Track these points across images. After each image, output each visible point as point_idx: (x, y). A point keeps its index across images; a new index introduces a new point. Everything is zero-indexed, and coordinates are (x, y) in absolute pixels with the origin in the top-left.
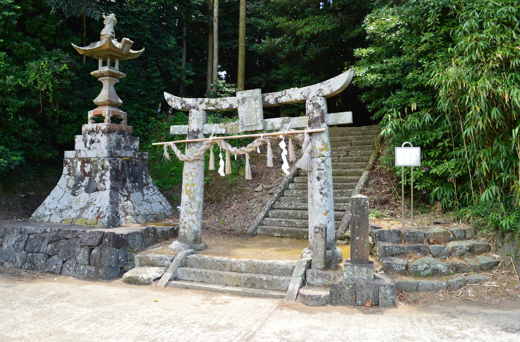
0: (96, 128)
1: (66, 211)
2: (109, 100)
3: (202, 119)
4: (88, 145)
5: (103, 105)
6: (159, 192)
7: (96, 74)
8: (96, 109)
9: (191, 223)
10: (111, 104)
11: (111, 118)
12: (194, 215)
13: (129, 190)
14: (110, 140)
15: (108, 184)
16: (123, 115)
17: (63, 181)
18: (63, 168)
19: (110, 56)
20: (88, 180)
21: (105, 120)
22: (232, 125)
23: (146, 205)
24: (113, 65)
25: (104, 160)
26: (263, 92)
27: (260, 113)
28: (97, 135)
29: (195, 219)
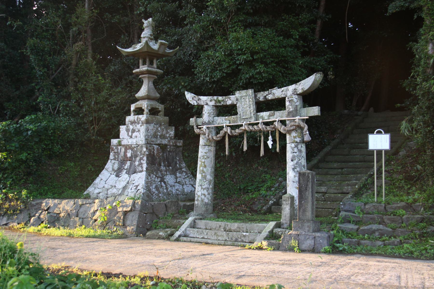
0: (137, 120)
1: (111, 190)
2: (147, 95)
3: (212, 113)
4: (130, 134)
5: (143, 98)
6: (192, 176)
7: (137, 72)
8: (138, 103)
9: (203, 197)
10: (147, 98)
11: (150, 111)
12: (205, 191)
13: (163, 173)
14: (147, 130)
15: (145, 166)
16: (160, 108)
17: (109, 165)
18: (110, 154)
19: (148, 55)
20: (129, 164)
21: (145, 113)
22: (234, 118)
23: (177, 186)
24: (151, 63)
25: (142, 147)
26: (255, 92)
27: (253, 108)
28: (137, 125)
29: (206, 193)
